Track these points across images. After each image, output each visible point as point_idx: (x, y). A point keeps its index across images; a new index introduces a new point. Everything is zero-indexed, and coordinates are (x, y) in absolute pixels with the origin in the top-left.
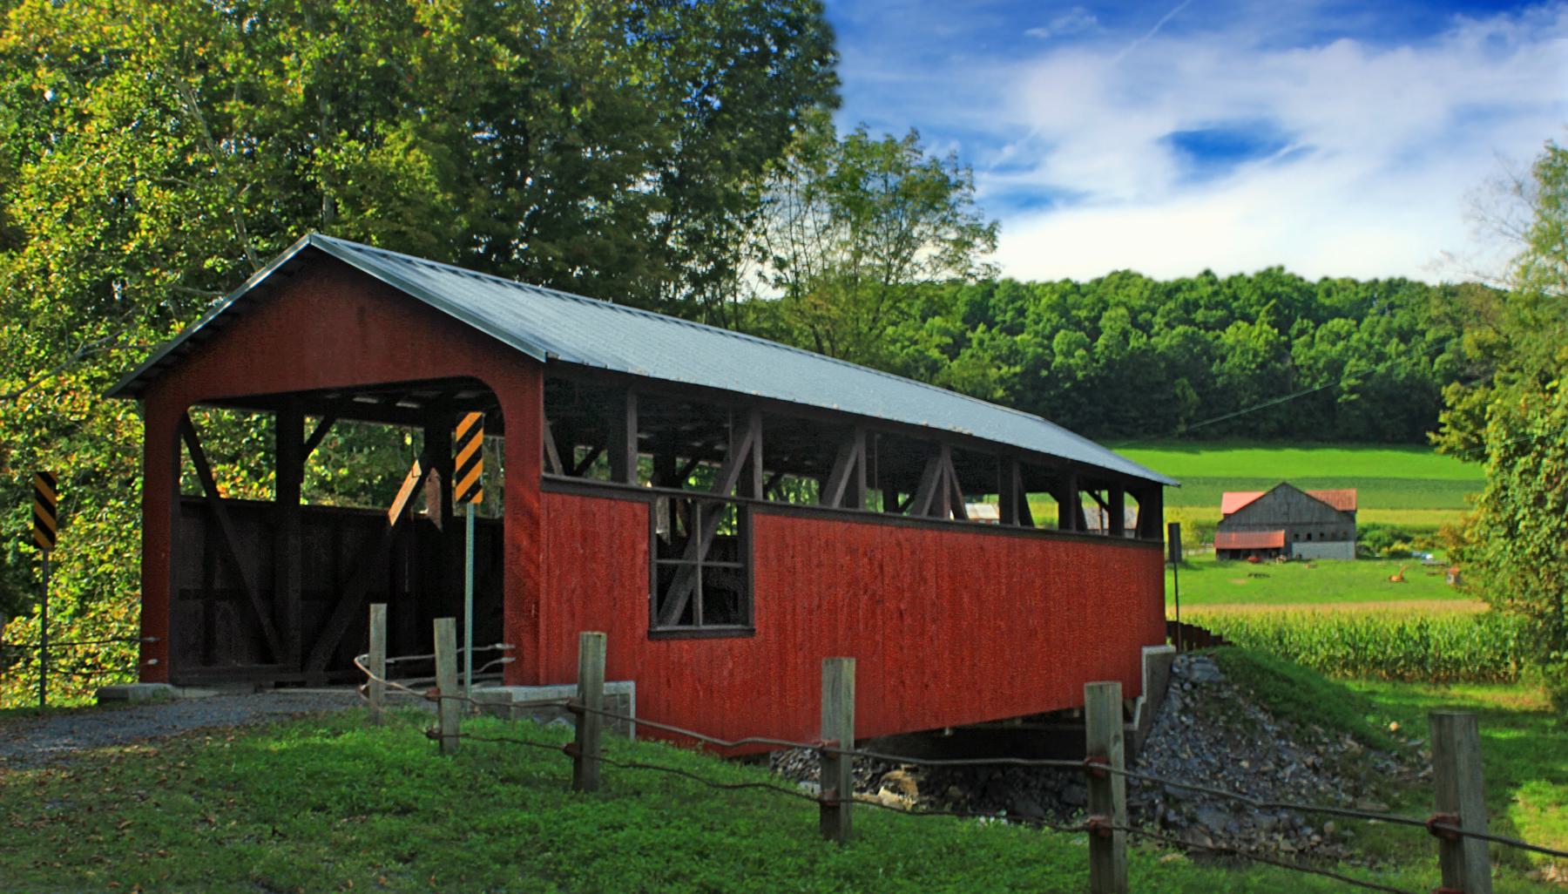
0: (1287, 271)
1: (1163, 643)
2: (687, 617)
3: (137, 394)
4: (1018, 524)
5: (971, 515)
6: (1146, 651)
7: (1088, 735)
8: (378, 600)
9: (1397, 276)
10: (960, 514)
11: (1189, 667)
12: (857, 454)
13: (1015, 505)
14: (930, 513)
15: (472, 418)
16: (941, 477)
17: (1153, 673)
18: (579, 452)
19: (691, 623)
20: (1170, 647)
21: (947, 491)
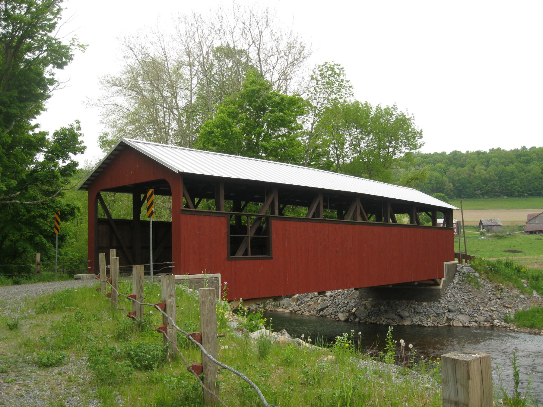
0: (58, 129)
1: (454, 260)
2: (246, 253)
3: (87, 189)
4: (416, 224)
5: (398, 222)
6: (445, 263)
7: (118, 265)
8: (113, 248)
9: (417, 125)
10: (394, 220)
11: (462, 268)
12: (320, 199)
13: (415, 217)
14: (313, 216)
15: (151, 191)
16: (356, 208)
17: (448, 270)
18: (196, 200)
19: (247, 255)
20: (456, 261)
21: (358, 212)
